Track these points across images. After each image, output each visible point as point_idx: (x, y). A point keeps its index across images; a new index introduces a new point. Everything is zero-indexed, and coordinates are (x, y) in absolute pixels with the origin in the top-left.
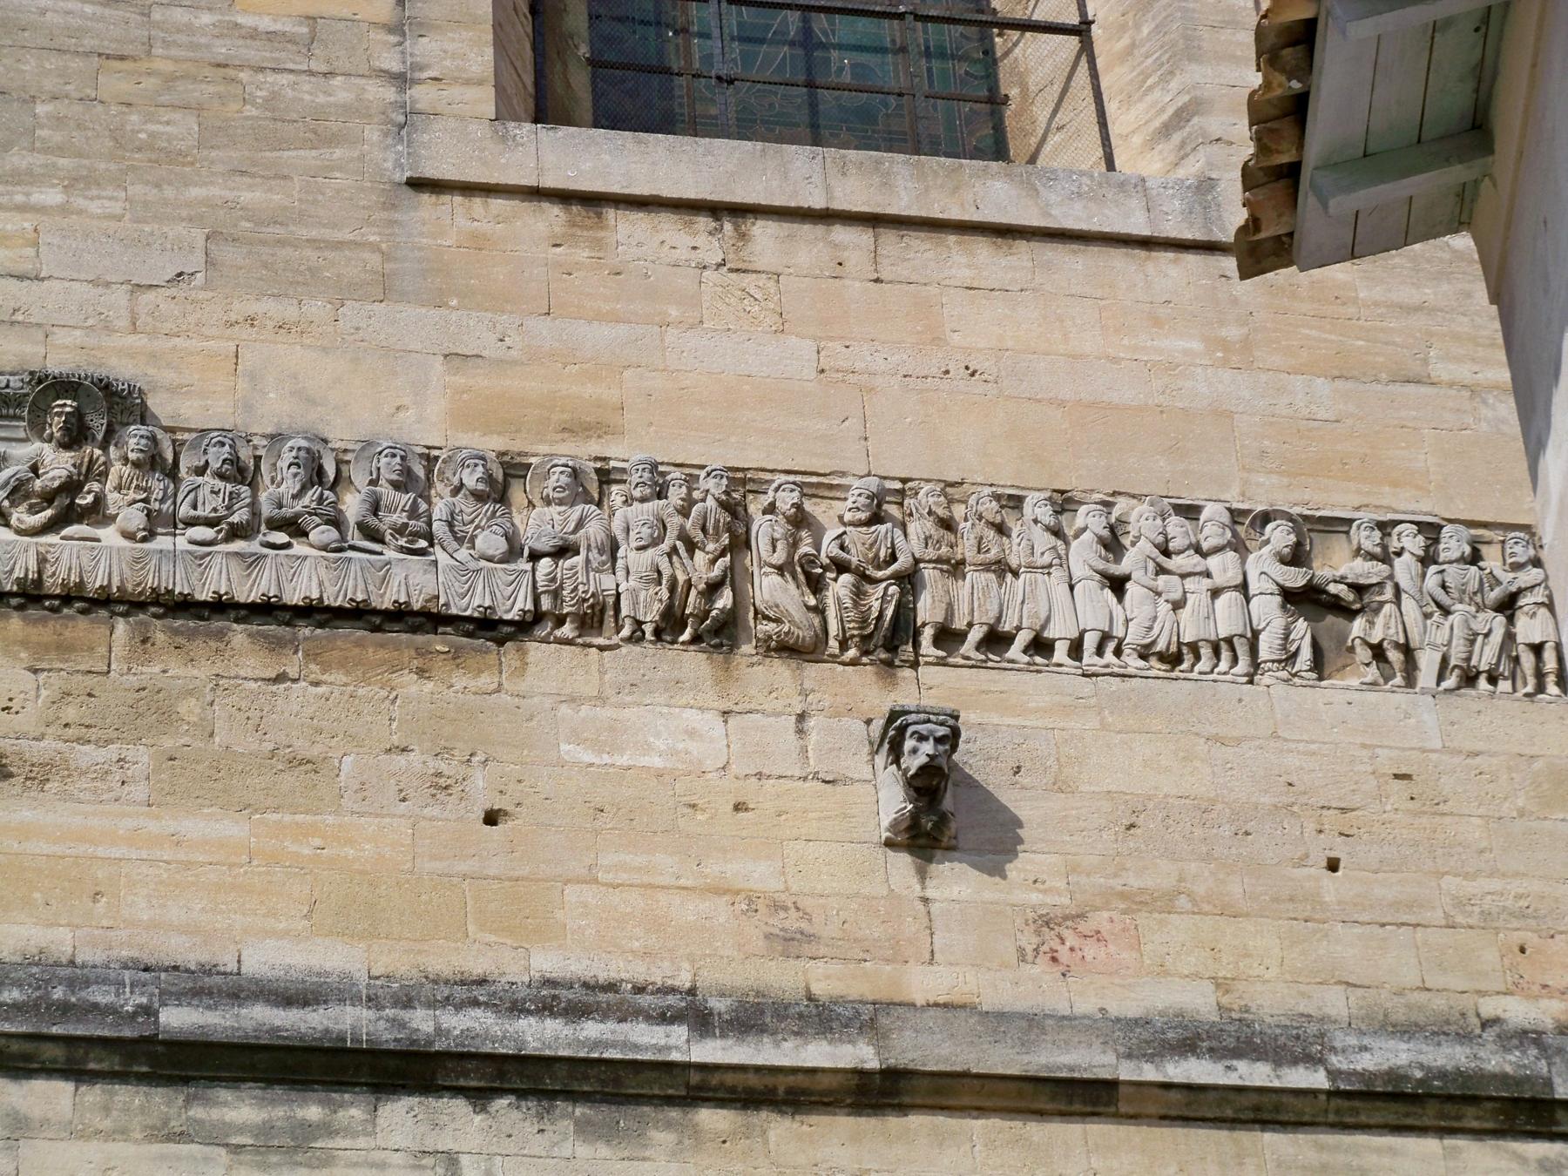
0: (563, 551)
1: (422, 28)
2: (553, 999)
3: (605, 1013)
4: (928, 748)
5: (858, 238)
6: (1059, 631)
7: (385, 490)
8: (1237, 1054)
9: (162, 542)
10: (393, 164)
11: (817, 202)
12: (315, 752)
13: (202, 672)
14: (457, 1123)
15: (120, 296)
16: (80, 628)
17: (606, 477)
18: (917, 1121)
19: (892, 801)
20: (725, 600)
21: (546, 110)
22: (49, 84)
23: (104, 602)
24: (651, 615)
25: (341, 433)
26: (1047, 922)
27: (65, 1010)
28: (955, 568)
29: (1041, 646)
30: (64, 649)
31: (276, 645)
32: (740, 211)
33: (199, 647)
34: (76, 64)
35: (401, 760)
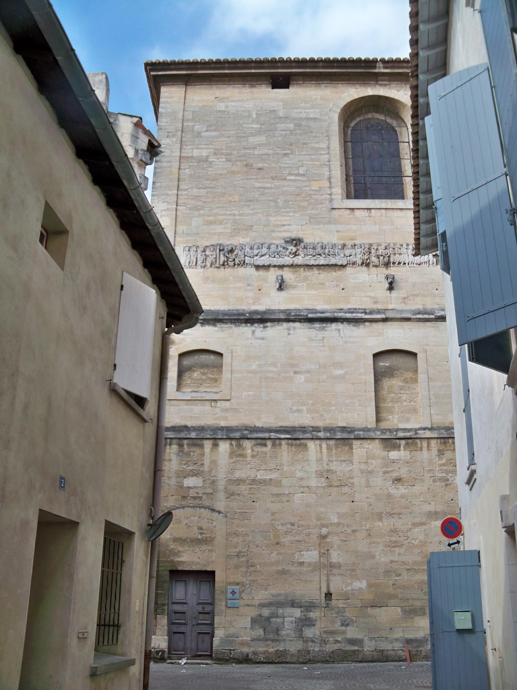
0: (350, 256)
1: (333, 187)
2: (350, 311)
3: (355, 313)
4: (391, 280)
5: (383, 211)
6: (407, 262)
7: (330, 249)
8: (424, 314)
9: (306, 258)
10: (329, 206)
11: (379, 207)
12: (323, 282)
13: (311, 273)
14: (340, 326)
15: (300, 226)
16: (298, 269)
17: (355, 245)
18: (389, 323)
19: (387, 285)
20: (368, 261)
21: (348, 197)
22: (291, 199)
23: (300, 266)
24: (360, 263)
25: (325, 243)
26: (404, 298)
27: (298, 315)
28: (395, 254)
29: (404, 264)
30: (296, 272)
31: (319, 269)
32: (370, 209)
33: (311, 270)
34: (293, 196)
35: (333, 283)
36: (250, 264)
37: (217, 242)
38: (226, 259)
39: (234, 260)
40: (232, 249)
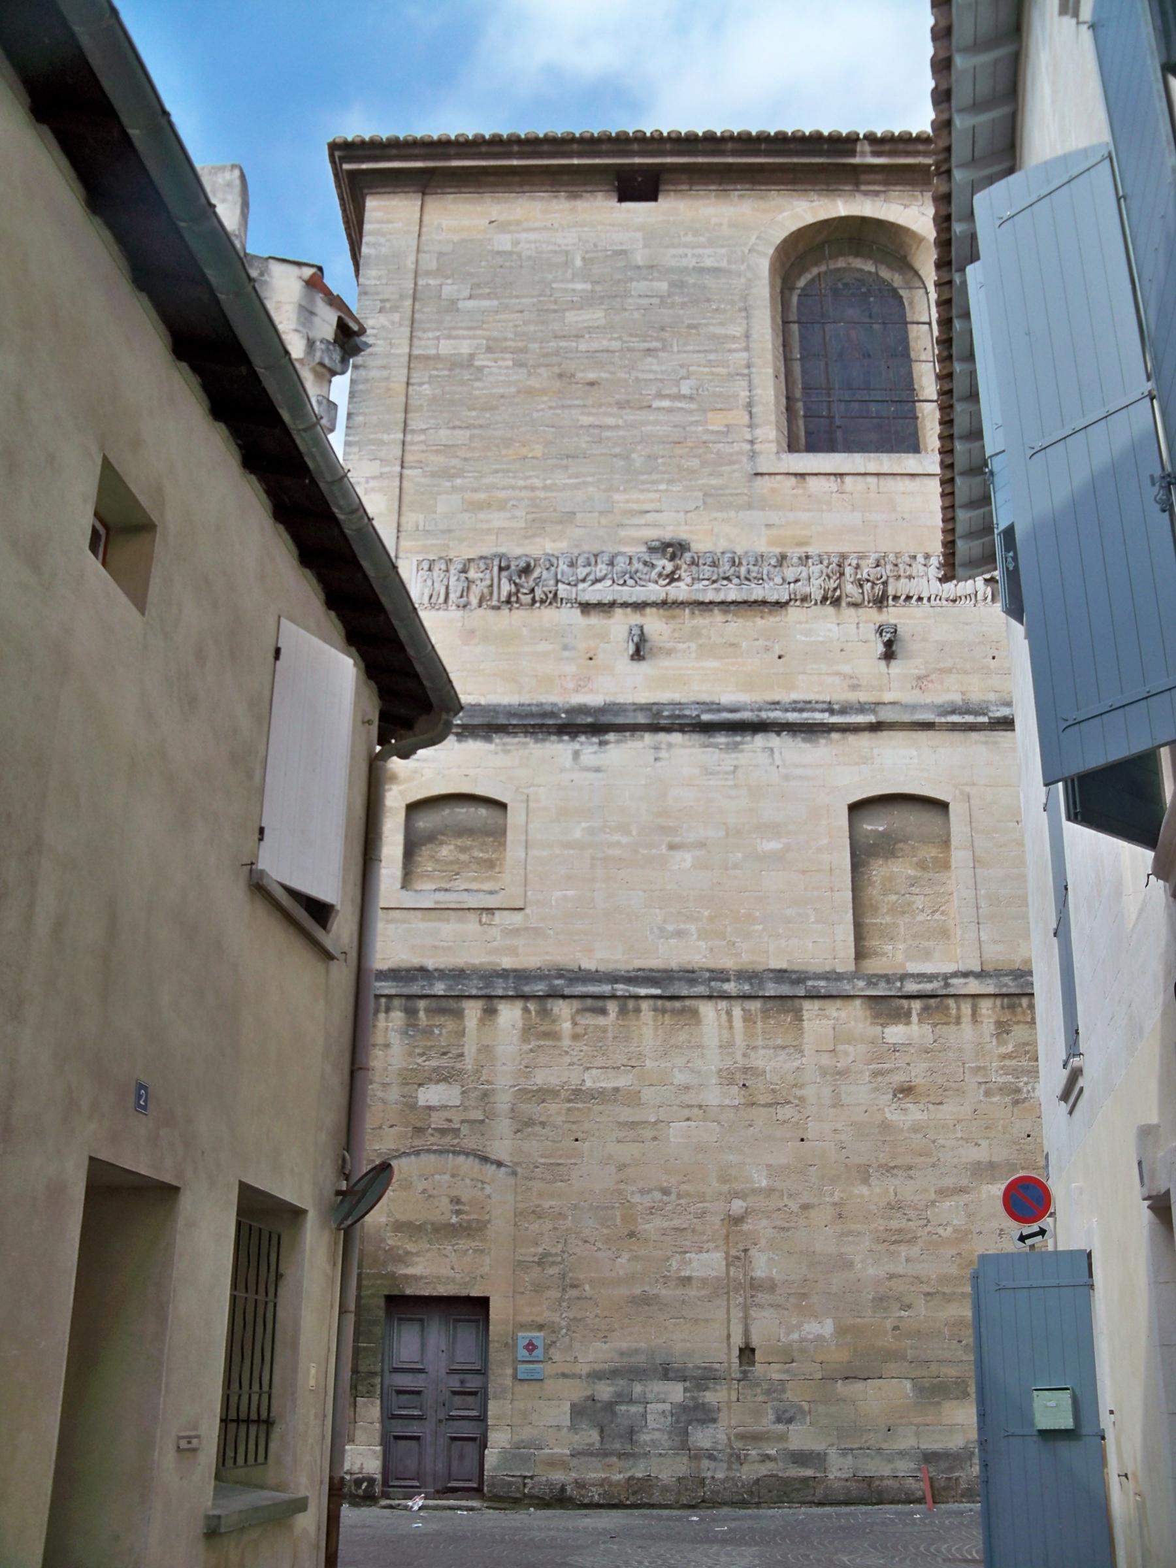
0: (797, 581)
1: (757, 426)
2: (797, 707)
3: (808, 710)
4: (889, 635)
5: (872, 480)
6: (925, 595)
7: (751, 567)
8: (965, 713)
9: (696, 586)
10: (749, 468)
11: (863, 471)
12: (736, 642)
13: (707, 621)
14: (774, 740)
15: (682, 514)
16: (677, 612)
17: (807, 557)
18: (885, 733)
19: (881, 649)
20: (838, 593)
21: (792, 447)
22: (661, 453)
23: (682, 604)
24: (819, 598)
26: (919, 678)
27: (679, 717)
28: (898, 577)
29: (920, 599)
30: (674, 617)
31: (725, 612)
32: (841, 475)
33: (707, 614)
34: (667, 446)
35: (757, 643)
36: (569, 601)
37: (494, 550)
38: (513, 589)
39: (532, 591)
40: (528, 565)
